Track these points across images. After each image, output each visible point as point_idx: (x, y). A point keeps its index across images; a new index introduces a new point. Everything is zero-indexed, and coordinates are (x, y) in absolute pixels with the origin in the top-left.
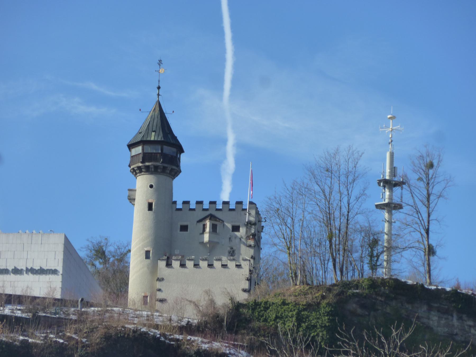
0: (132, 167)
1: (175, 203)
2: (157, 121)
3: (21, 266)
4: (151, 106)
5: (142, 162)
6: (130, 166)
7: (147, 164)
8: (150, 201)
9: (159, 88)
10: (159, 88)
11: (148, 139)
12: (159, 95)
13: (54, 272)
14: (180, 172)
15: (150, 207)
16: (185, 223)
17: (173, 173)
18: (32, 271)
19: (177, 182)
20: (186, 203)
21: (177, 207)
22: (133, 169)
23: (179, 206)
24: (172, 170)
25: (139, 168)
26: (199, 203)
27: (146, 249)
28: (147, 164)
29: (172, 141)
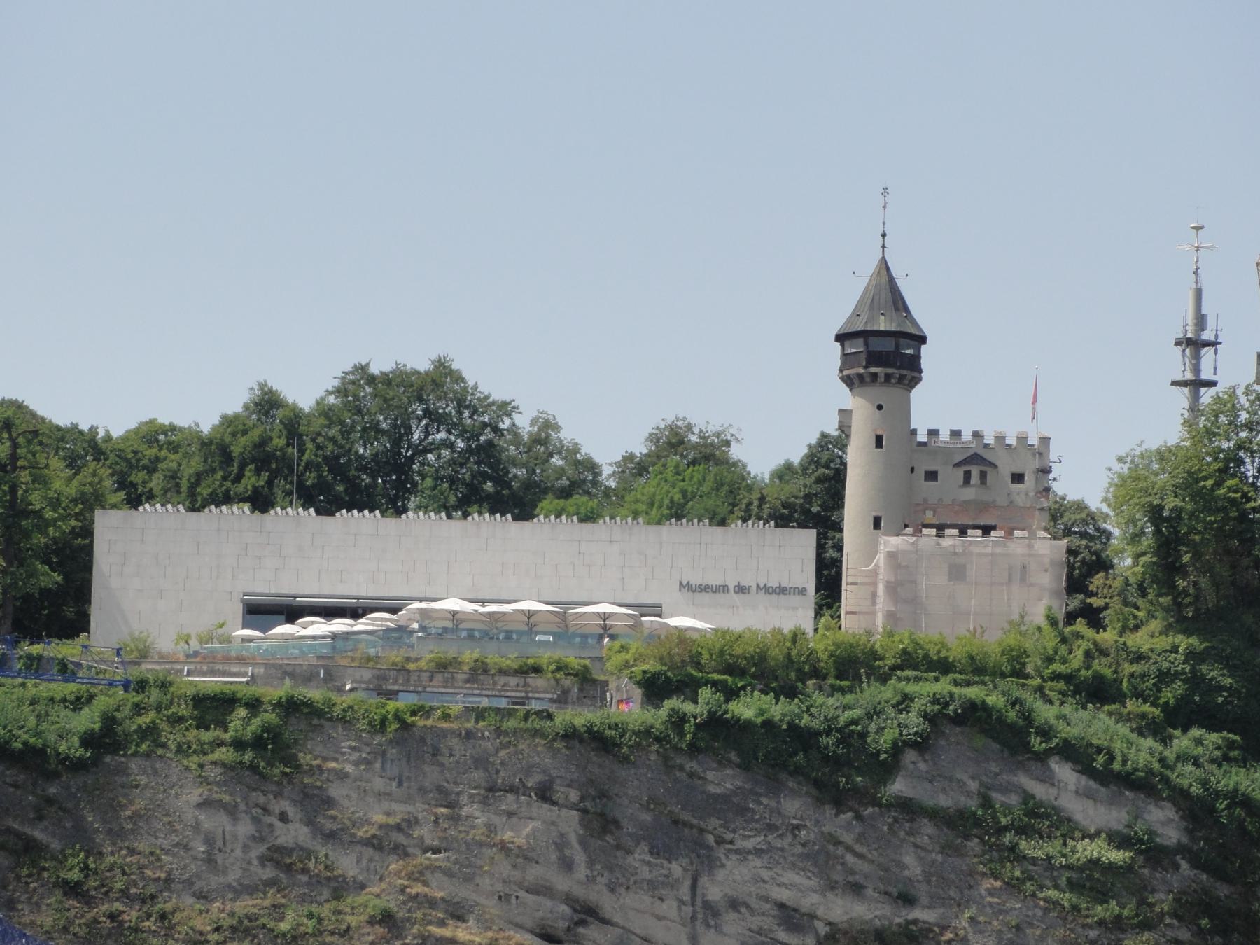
0: (846, 373)
1: (914, 432)
2: (886, 295)
3: (749, 581)
4: (871, 266)
5: (866, 367)
6: (841, 371)
7: (873, 370)
8: (879, 433)
9: (884, 235)
10: (884, 235)
11: (875, 328)
12: (883, 247)
13: (803, 592)
14: (920, 380)
15: (879, 441)
16: (932, 468)
17: (906, 382)
18: (768, 590)
19: (917, 394)
20: (933, 433)
21: (919, 439)
22: (848, 377)
23: (922, 437)
24: (913, 378)
25: (860, 376)
26: (956, 434)
27: (875, 514)
28: (873, 370)
29: (914, 331)
